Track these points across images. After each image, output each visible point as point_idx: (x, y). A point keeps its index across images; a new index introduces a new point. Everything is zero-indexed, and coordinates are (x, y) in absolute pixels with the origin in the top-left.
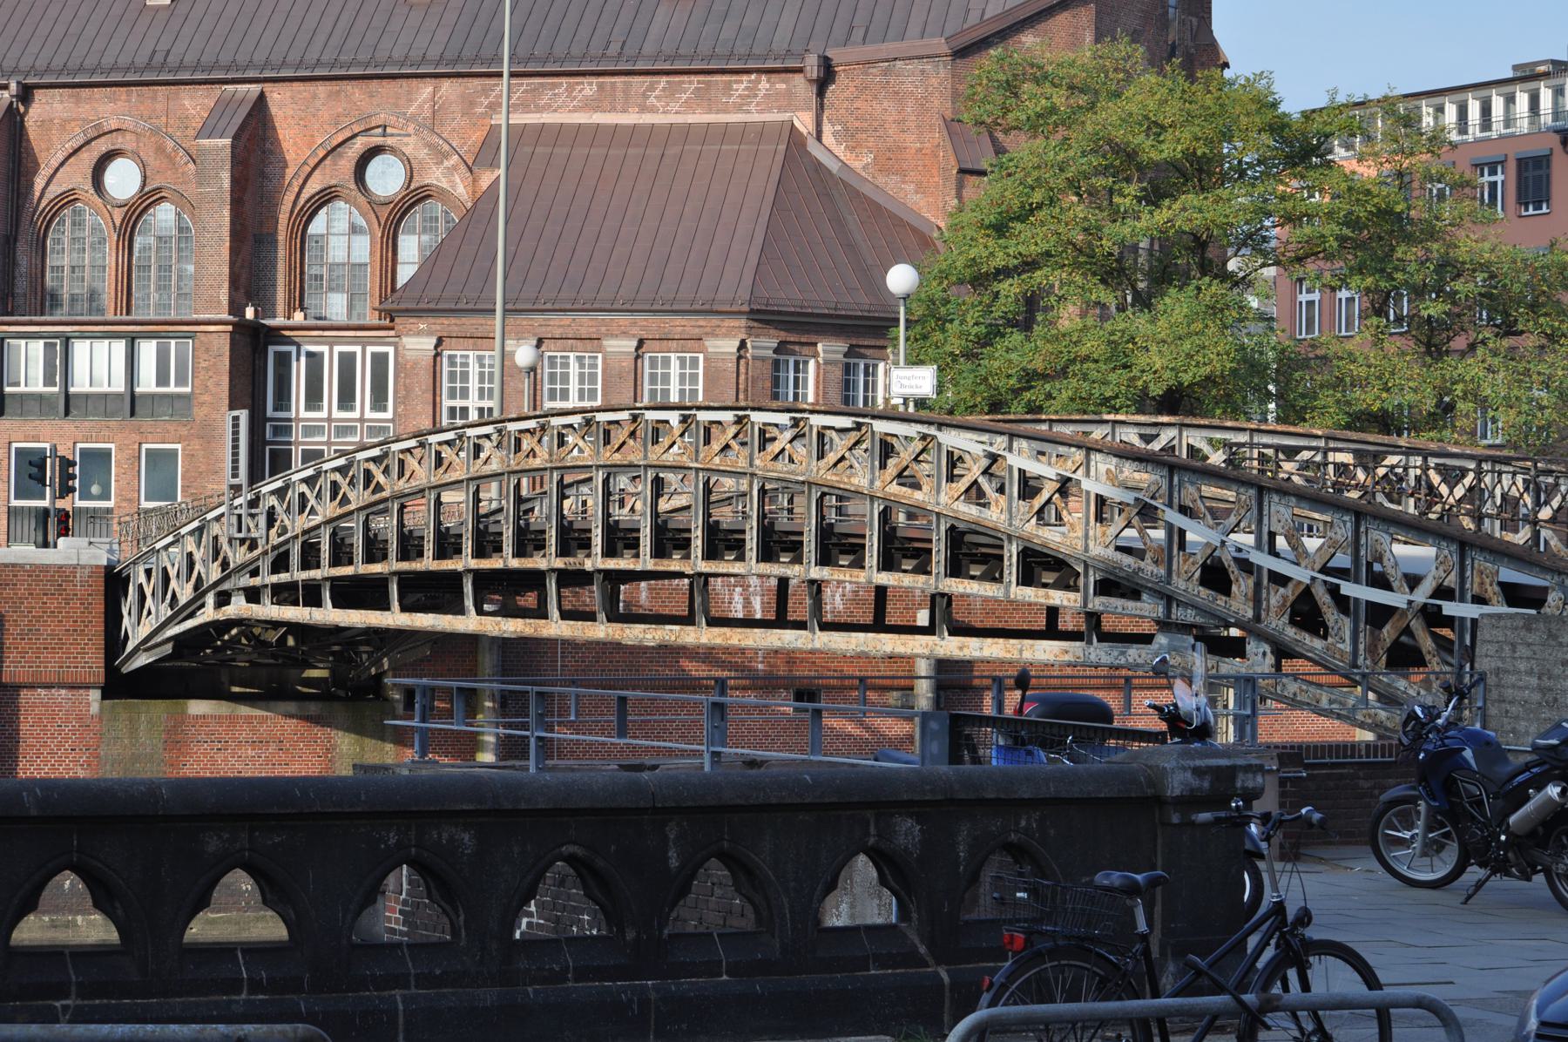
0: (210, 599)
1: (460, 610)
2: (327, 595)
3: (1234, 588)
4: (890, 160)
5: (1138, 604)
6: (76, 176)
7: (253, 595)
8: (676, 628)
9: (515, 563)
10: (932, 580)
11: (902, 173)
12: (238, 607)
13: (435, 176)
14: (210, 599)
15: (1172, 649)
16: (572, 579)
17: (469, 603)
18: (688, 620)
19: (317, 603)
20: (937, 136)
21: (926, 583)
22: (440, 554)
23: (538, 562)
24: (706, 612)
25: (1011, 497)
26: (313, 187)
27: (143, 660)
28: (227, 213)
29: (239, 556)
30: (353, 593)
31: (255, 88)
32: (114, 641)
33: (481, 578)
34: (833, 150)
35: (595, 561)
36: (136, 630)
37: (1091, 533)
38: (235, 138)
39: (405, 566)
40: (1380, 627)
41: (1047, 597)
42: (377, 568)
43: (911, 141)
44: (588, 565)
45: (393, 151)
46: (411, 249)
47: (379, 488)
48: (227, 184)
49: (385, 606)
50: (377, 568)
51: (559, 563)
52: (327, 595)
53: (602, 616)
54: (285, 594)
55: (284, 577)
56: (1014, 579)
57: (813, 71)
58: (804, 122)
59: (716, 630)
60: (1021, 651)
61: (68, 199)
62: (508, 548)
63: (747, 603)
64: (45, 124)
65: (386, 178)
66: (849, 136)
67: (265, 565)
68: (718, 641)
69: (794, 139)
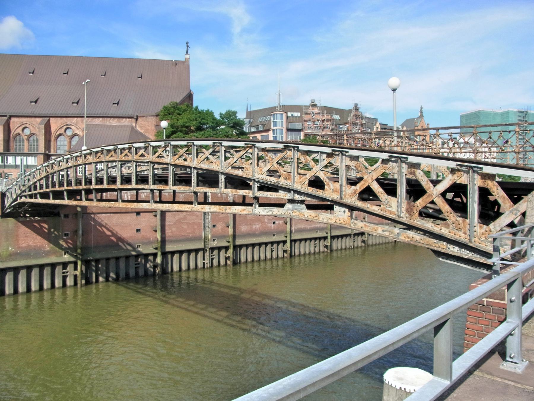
0: (19, 198)
1: (64, 199)
2: (39, 196)
3: (326, 187)
4: (147, 131)
5: (278, 194)
6: (19, 131)
7: (26, 196)
8: (113, 203)
9: (75, 188)
10: (192, 188)
11: (149, 133)
12: (23, 199)
13: (77, 132)
14: (19, 198)
15: (294, 210)
16: (88, 192)
17: (66, 197)
18: (116, 201)
19: (36, 198)
20: (153, 128)
21: (190, 189)
22: (60, 186)
23: (81, 187)
24: (121, 198)
25: (222, 161)
26: (58, 133)
27: (8, 211)
28: (44, 137)
29: (23, 189)
30: (45, 196)
31: (48, 118)
32: (3, 207)
33: (69, 192)
34: (138, 128)
35: (93, 186)
36: (7, 204)
37: (255, 170)
38: (45, 125)
39: (53, 189)
40: (415, 200)
41: (237, 192)
42: (48, 190)
43: (150, 128)
44: (91, 187)
45: (70, 128)
46: (73, 143)
47: (48, 172)
48: (44, 132)
49: (49, 198)
50: (48, 190)
51: (85, 187)
52: (39, 196)
53: (95, 200)
54: (31, 196)
55: (31, 193)
56: (223, 186)
57: (135, 117)
58: (134, 125)
59: (124, 203)
60: (226, 210)
61: (18, 134)
62: (73, 184)
63: (127, 197)
64: (14, 122)
65: (69, 133)
66: (140, 127)
67: (27, 190)
68: (124, 206)
69: (133, 128)
